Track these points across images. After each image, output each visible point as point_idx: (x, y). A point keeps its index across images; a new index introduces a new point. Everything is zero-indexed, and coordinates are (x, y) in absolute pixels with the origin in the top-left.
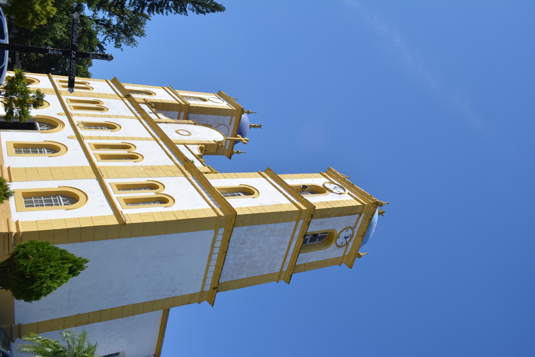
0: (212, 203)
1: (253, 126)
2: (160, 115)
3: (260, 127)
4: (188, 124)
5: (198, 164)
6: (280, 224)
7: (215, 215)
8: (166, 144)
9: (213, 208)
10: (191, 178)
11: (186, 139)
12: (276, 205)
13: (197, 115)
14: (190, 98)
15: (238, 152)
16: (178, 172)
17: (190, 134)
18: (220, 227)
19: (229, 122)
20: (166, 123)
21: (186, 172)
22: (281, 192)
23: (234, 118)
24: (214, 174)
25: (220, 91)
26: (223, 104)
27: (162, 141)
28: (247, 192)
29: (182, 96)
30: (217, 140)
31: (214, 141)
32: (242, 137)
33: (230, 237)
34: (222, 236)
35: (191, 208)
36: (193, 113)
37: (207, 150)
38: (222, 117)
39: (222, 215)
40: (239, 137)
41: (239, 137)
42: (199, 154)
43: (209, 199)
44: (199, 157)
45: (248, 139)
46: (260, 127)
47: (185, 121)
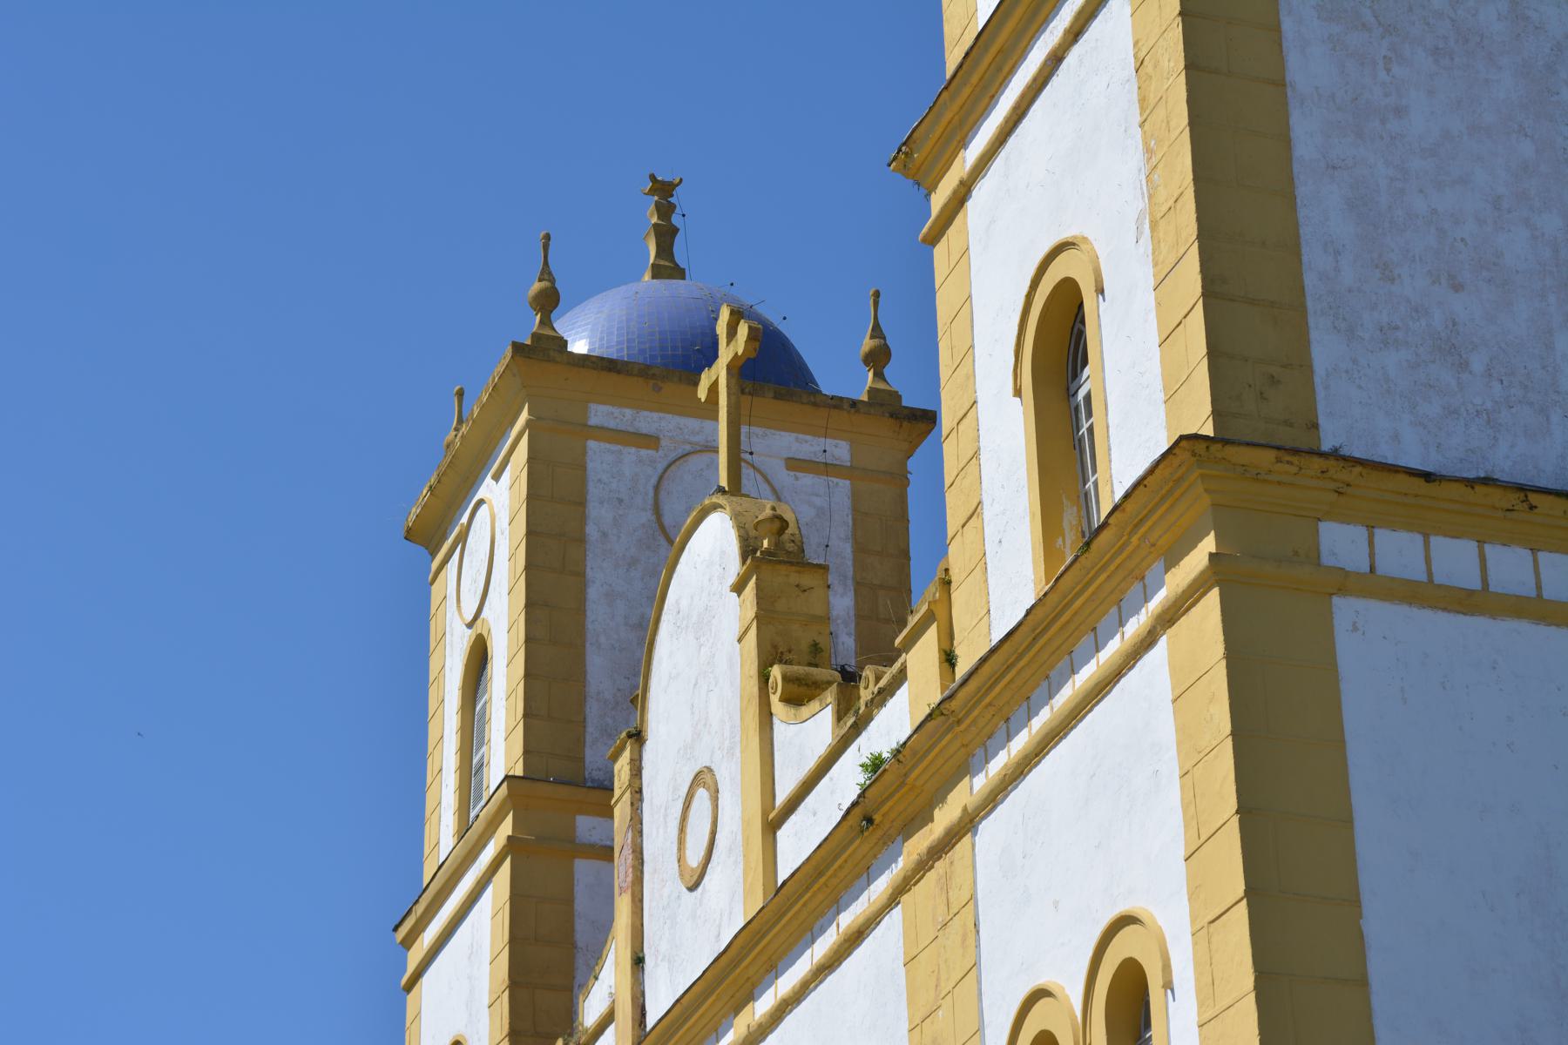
0: (1135, 626)
1: (665, 249)
2: (591, 1009)
3: (663, 190)
4: (638, 793)
5: (892, 726)
6: (1293, 60)
7: (1211, 605)
8: (774, 969)
9: (1168, 618)
10: (980, 783)
11: (737, 811)
12: (1142, 101)
13: (593, 710)
14: (470, 771)
15: (878, 358)
16: (946, 884)
17: (704, 779)
18: (1314, 557)
19: (630, 454)
20: (638, 961)
21: (945, 816)
22: (1055, 60)
23: (600, 414)
24: (957, 596)
25: (410, 535)
26: (501, 500)
27: (751, 997)
28: (1060, 342)
29: (464, 828)
30: (734, 567)
31: (738, 588)
32: (710, 356)
33: (1394, 469)
34: (1381, 535)
35: (1172, 795)
36: (580, 741)
37: (829, 629)
38: (599, 514)
39: (1209, 544)
40: (714, 388)
41: (714, 388)
42: (828, 715)
43: (1113, 648)
44: (853, 724)
45: (725, 314)
46: (663, 190)
47: (621, 811)
